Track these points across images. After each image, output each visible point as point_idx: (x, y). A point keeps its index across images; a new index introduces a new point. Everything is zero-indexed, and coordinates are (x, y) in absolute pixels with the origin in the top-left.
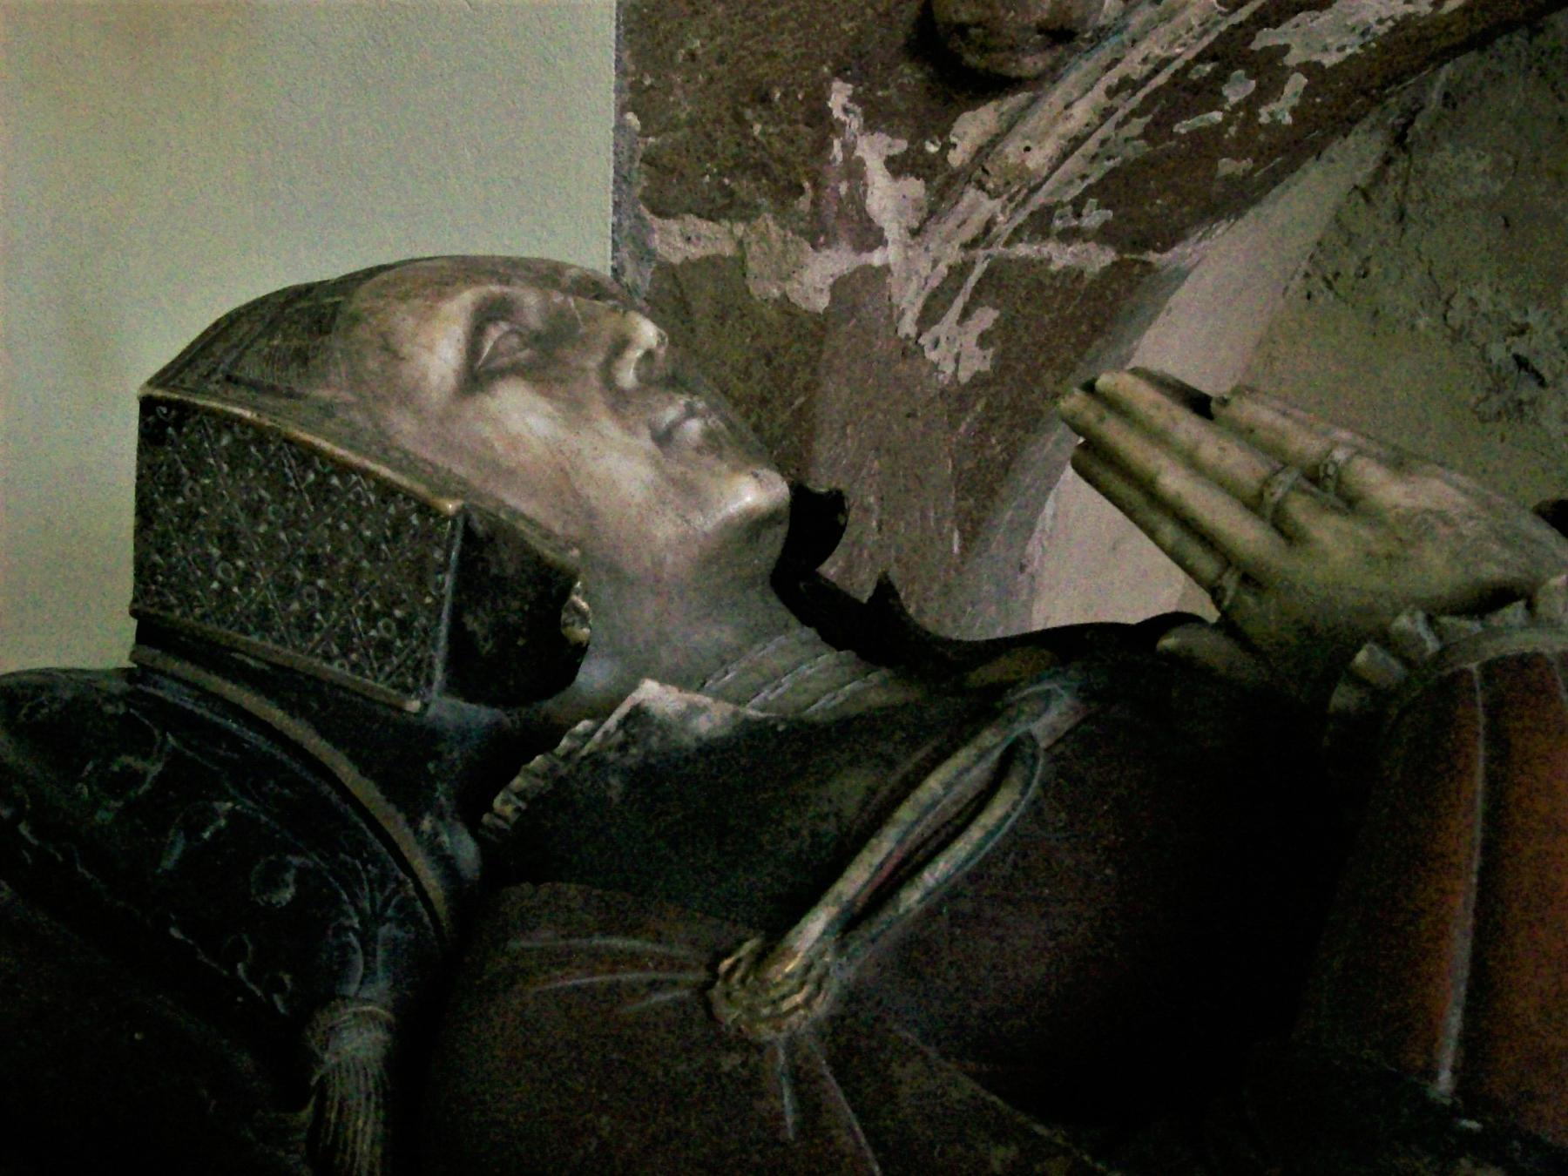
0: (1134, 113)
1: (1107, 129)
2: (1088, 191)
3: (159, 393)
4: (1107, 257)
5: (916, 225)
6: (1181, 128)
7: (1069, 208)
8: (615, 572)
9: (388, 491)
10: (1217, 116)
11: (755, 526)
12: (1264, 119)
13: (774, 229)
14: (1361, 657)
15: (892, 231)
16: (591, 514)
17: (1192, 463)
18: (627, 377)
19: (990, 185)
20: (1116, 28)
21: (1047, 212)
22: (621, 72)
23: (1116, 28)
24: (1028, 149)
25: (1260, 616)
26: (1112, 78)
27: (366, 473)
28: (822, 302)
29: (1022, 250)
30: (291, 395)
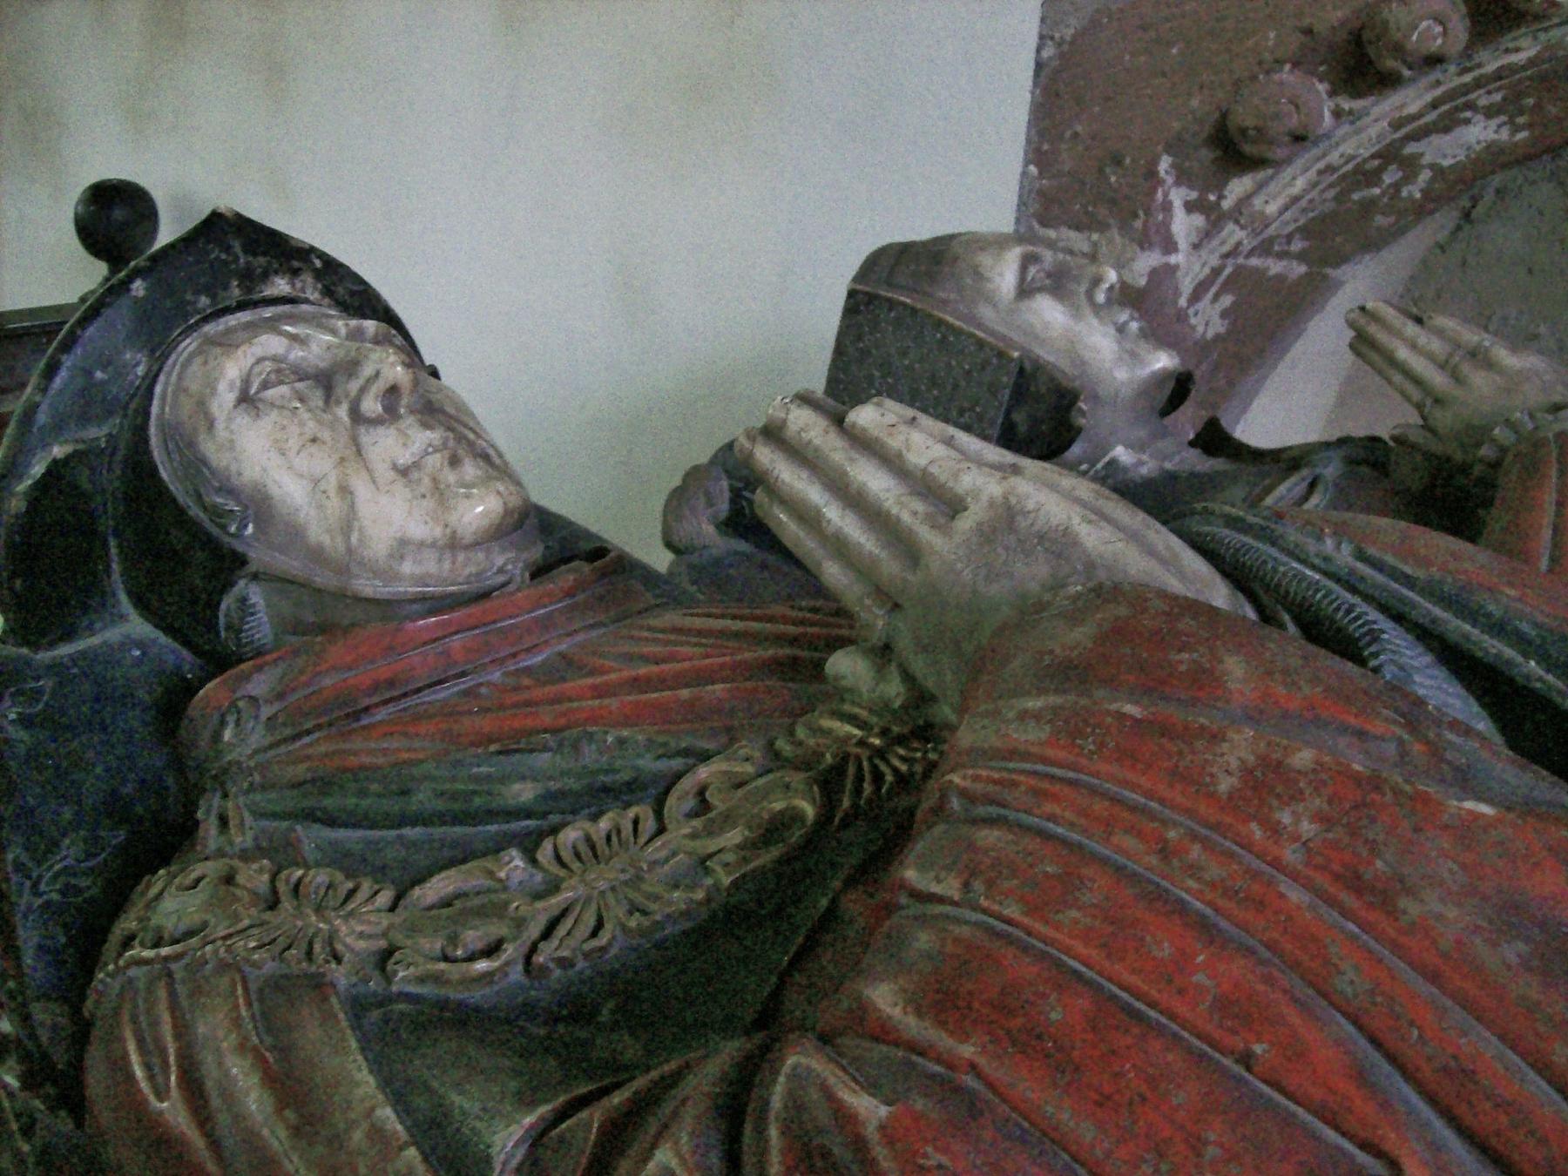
0: (1331, 186)
1: (1314, 194)
2: (1298, 229)
3: (859, 287)
4: (1302, 269)
5: (1196, 241)
6: (1356, 196)
7: (1284, 240)
8: (1095, 398)
9: (981, 344)
10: (1377, 191)
11: (1161, 378)
12: (1404, 193)
13: (1118, 239)
14: (1497, 431)
15: (1183, 244)
16: (1083, 363)
17: (1413, 346)
18: (1101, 297)
19: (1242, 222)
20: (1327, 136)
21: (1270, 241)
22: (1029, 141)
23: (1327, 136)
24: (1267, 202)
25: (1444, 419)
26: (1321, 165)
27: (972, 335)
28: (1143, 282)
29: (1254, 262)
30: (925, 293)
